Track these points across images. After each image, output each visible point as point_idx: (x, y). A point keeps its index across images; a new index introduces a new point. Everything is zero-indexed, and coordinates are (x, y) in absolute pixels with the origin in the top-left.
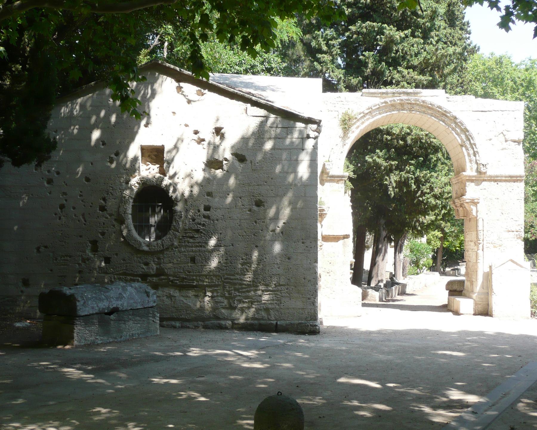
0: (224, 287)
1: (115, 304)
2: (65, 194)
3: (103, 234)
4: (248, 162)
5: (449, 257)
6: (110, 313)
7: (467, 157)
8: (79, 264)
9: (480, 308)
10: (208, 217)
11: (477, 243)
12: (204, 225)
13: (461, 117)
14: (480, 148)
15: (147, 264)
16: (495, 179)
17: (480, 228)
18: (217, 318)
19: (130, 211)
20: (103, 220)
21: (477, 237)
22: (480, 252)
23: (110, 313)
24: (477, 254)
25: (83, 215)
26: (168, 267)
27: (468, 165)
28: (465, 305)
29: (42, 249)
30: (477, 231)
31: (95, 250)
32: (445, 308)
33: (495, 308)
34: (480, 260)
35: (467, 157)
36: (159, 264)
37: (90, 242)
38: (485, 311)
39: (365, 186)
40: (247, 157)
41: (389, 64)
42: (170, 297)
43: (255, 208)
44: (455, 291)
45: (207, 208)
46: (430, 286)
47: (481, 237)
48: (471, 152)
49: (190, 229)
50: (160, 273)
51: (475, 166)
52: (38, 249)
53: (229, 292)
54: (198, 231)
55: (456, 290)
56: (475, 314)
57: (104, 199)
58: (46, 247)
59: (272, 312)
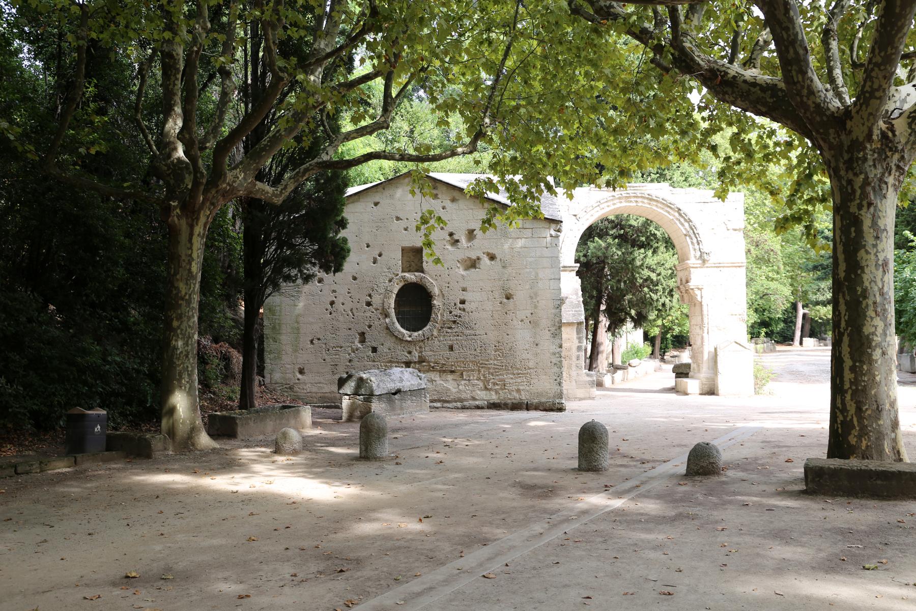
0: (479, 371)
1: (398, 385)
2: (334, 291)
3: (370, 326)
4: (498, 259)
5: (669, 341)
6: (394, 394)
7: (691, 246)
8: (349, 354)
9: (706, 389)
10: (464, 310)
11: (701, 327)
12: (460, 317)
13: (684, 209)
14: (702, 237)
15: (410, 353)
16: (718, 266)
17: (705, 312)
18: (474, 399)
19: (393, 306)
20: (369, 314)
21: (702, 320)
22: (705, 335)
23: (394, 394)
24: (702, 338)
25: (351, 310)
26: (427, 353)
27: (692, 252)
28: (692, 385)
29: (315, 341)
30: (702, 315)
31: (363, 341)
32: (673, 390)
33: (722, 386)
34: (706, 343)
35: (691, 246)
36: (421, 352)
37: (359, 334)
38: (711, 391)
39: (588, 269)
40: (497, 255)
41: (594, 109)
42: (432, 381)
43: (505, 300)
44: (682, 373)
45: (463, 302)
46: (654, 373)
47: (705, 321)
48: (695, 241)
49: (448, 320)
50: (421, 361)
51: (698, 254)
52: (312, 342)
53: (484, 375)
54: (454, 322)
55: (682, 372)
56: (701, 394)
57: (370, 296)
58: (319, 339)
59: (522, 393)
